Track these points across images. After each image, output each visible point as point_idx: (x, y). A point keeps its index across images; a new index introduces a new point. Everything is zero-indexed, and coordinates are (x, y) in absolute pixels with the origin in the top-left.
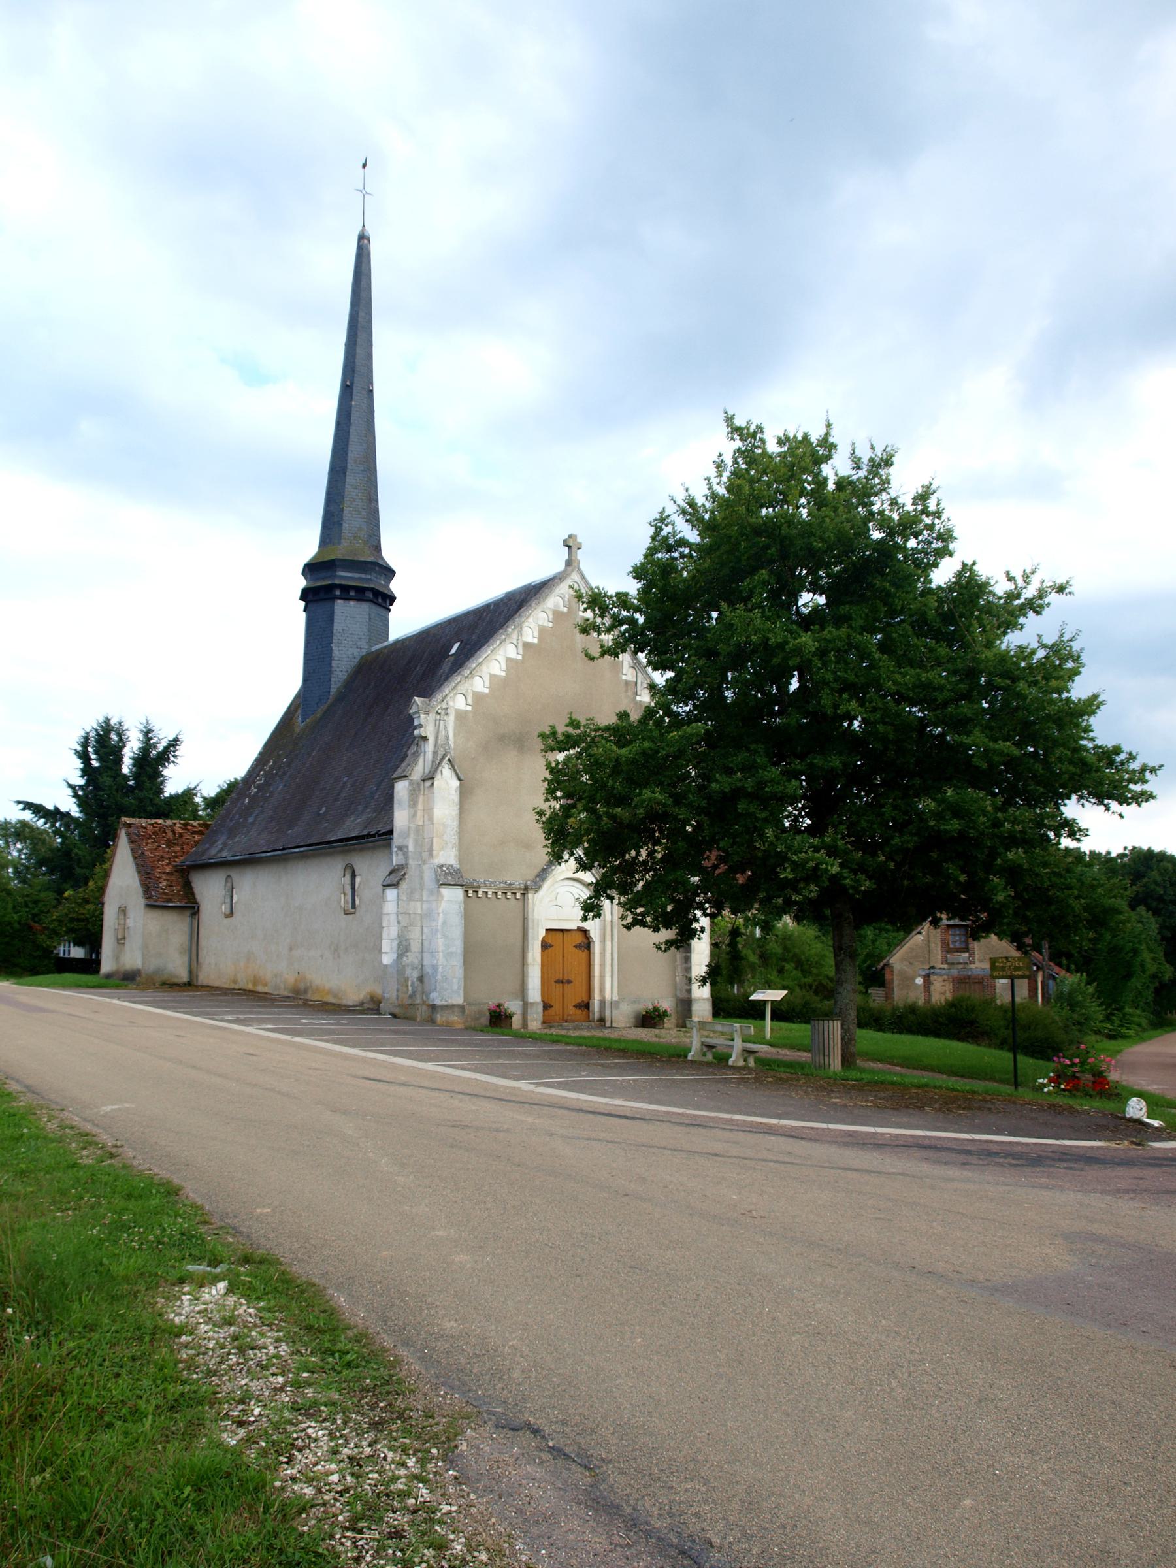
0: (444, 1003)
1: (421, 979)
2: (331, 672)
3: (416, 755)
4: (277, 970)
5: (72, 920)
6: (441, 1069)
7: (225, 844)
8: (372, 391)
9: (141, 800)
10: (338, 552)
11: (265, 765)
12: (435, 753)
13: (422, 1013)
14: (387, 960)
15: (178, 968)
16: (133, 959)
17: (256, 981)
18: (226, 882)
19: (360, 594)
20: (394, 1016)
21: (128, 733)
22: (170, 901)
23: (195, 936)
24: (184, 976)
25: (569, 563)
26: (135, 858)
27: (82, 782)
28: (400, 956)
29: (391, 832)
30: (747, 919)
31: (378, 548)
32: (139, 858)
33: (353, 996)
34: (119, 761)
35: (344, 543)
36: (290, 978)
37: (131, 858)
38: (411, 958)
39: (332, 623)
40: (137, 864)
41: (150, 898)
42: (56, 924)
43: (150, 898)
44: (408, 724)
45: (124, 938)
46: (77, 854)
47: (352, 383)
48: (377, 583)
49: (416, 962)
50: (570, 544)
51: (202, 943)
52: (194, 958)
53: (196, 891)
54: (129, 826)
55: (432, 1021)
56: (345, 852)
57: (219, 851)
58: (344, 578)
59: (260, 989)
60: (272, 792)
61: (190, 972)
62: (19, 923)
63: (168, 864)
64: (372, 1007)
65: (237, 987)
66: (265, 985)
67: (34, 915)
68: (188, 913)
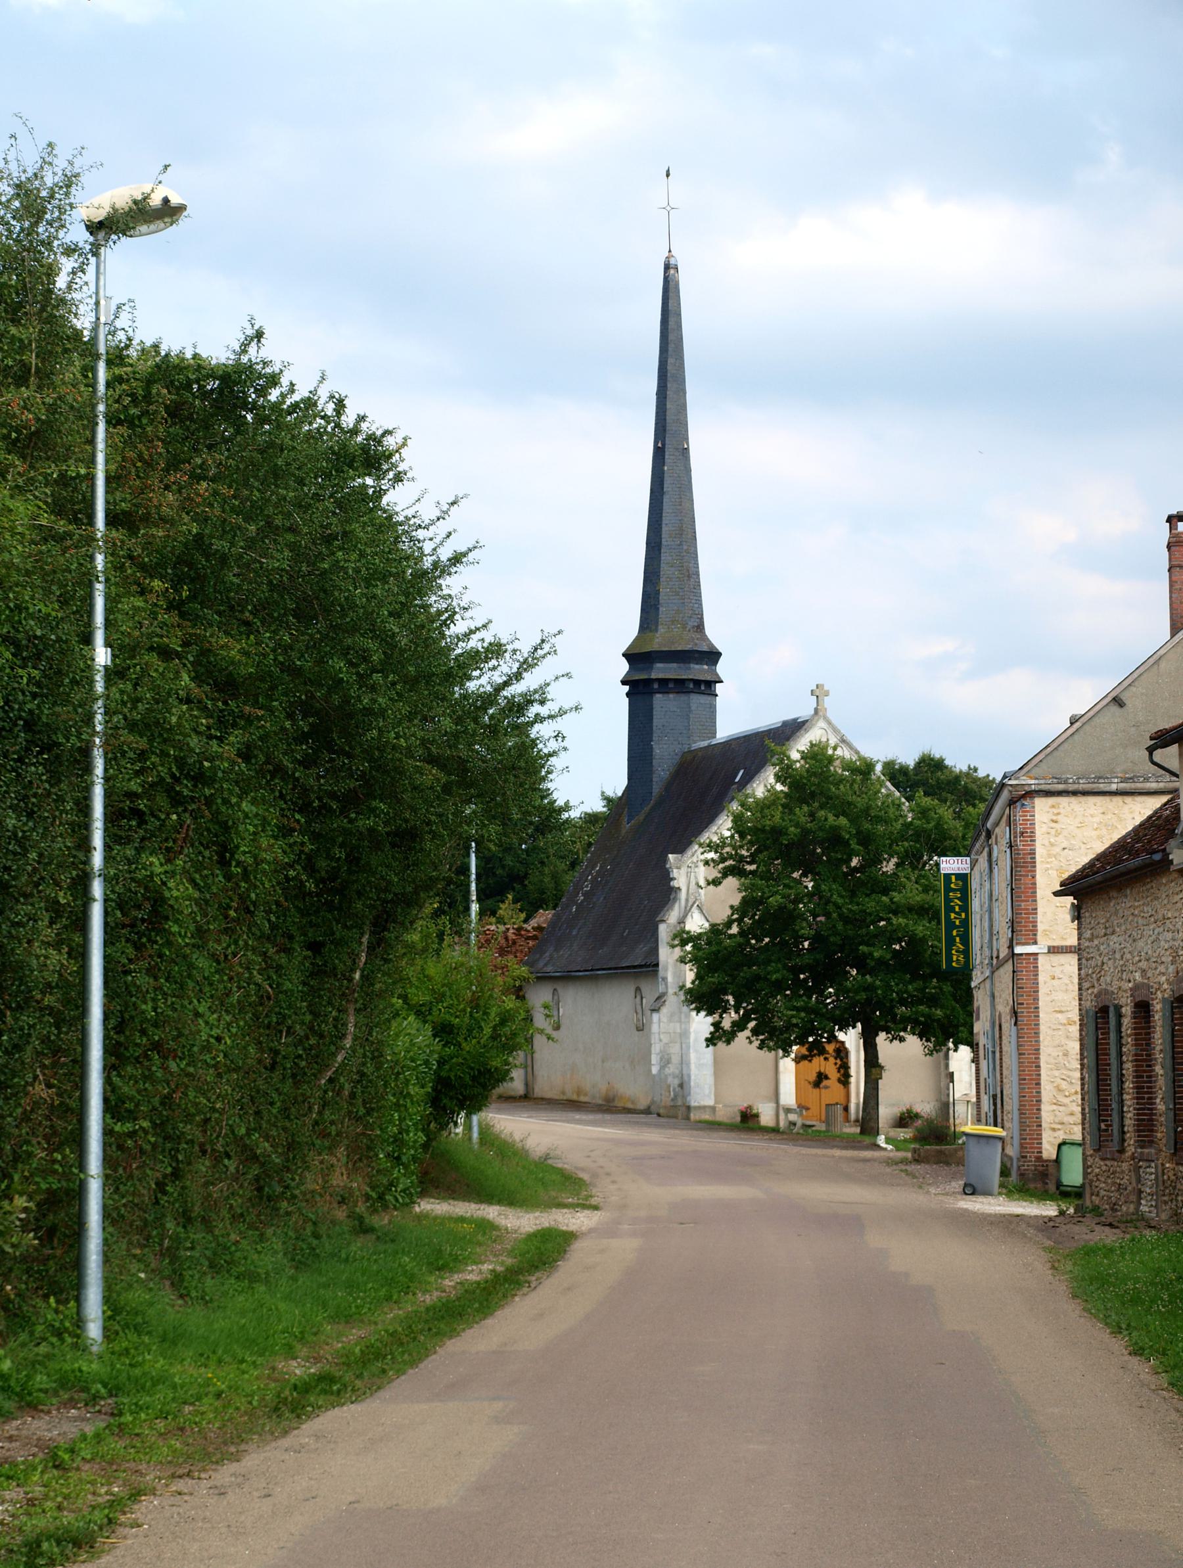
1: (681, 1086)
2: (651, 772)
3: (675, 899)
4: (594, 1083)
7: (551, 957)
8: (687, 449)
10: (658, 642)
11: (593, 868)
12: (687, 900)
13: (681, 1112)
14: (655, 1070)
19: (680, 686)
20: (659, 1115)
25: (816, 711)
28: (662, 1068)
29: (657, 965)
30: (829, 1042)
31: (700, 627)
33: (642, 1104)
35: (662, 629)
36: (603, 1087)
38: (672, 1069)
39: (652, 719)
44: (666, 877)
47: (664, 445)
48: (698, 671)
49: (677, 1072)
50: (818, 693)
52: (999, 1106)
55: (688, 1118)
56: (637, 976)
57: (546, 965)
59: (583, 1099)
61: (527, 1085)
64: (647, 1111)
66: (586, 1095)
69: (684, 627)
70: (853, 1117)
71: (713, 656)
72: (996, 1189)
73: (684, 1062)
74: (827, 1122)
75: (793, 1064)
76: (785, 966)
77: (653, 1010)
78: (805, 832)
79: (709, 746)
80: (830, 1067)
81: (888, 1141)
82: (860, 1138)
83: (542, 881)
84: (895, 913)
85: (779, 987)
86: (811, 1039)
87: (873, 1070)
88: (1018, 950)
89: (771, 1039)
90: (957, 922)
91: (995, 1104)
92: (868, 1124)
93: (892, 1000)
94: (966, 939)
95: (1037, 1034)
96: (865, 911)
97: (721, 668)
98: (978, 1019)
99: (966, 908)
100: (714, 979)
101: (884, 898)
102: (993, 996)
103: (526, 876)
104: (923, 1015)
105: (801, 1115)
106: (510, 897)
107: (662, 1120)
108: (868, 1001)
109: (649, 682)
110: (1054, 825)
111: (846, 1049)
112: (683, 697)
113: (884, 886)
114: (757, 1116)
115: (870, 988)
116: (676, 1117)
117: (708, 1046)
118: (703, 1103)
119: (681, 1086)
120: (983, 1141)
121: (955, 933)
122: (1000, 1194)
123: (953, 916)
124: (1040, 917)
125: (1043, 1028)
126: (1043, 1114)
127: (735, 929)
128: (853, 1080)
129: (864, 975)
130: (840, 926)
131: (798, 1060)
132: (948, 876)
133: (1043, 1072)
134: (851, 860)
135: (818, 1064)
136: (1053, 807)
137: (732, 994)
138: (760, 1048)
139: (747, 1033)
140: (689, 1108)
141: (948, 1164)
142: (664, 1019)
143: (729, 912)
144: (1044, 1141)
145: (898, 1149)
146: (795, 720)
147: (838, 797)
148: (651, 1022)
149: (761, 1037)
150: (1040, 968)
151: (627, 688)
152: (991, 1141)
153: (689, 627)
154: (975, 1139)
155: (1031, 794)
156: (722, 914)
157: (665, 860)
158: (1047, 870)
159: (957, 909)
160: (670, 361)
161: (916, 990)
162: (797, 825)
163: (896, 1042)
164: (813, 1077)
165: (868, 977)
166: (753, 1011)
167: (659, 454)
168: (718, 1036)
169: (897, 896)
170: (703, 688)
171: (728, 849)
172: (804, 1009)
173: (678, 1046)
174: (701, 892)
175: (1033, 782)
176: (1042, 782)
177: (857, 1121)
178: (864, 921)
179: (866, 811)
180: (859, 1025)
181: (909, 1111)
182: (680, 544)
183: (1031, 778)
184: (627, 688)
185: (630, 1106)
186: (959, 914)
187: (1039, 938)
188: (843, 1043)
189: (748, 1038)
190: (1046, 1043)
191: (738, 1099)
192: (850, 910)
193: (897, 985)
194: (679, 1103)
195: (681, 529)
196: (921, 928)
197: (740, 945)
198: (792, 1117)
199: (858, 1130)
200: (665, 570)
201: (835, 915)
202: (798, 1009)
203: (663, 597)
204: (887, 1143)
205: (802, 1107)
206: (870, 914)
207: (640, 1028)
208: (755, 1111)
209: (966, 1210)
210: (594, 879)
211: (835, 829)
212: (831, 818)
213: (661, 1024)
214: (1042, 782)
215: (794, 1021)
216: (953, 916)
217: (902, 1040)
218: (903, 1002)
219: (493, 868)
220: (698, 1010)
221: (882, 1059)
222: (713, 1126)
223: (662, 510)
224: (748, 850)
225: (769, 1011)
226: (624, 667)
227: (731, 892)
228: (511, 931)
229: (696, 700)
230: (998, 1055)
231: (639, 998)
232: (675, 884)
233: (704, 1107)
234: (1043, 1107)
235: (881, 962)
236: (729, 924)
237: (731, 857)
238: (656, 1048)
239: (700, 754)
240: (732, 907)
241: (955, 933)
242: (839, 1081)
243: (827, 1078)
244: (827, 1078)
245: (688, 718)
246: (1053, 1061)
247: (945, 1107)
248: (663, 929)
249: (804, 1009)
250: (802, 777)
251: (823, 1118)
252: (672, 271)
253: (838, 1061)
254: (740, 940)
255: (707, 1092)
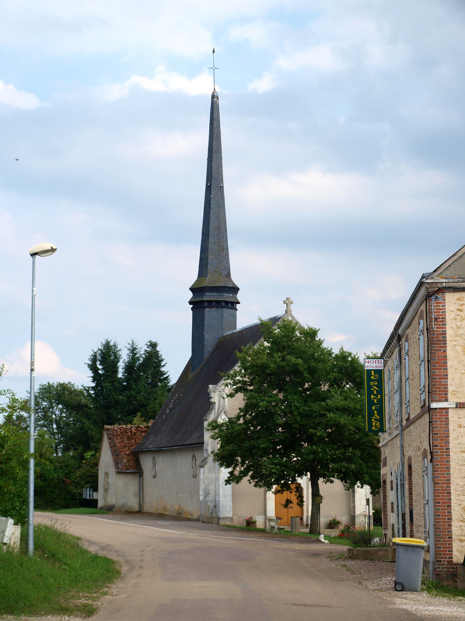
0: (223, 516)
1: (215, 506)
2: (203, 347)
3: (213, 409)
4: (172, 504)
5: (88, 477)
6: (173, 532)
8: (222, 187)
9: (129, 397)
10: (207, 283)
11: (174, 396)
12: (219, 409)
13: (215, 520)
14: (201, 498)
15: (134, 504)
16: (111, 500)
17: (165, 509)
18: (153, 460)
19: (218, 304)
20: (203, 522)
21: (120, 353)
22: (128, 469)
23: (141, 487)
24: (136, 508)
25: (286, 311)
26: (111, 447)
27: (93, 385)
29: (203, 443)
31: (228, 275)
32: (113, 446)
33: (195, 517)
34: (116, 372)
35: (209, 276)
36: (176, 507)
37: (109, 448)
38: (210, 498)
39: (204, 321)
40: (112, 451)
41: (118, 468)
42: (79, 479)
43: (118, 468)
45: (108, 489)
46: (90, 434)
47: (211, 184)
48: (227, 297)
49: (213, 499)
50: (288, 302)
51: (145, 491)
52: (141, 498)
53: (142, 464)
54: (108, 430)
55: (218, 524)
57: (149, 444)
58: (212, 295)
59: (167, 513)
60: (174, 413)
61: (140, 506)
62: (58, 479)
63: (128, 450)
64: (198, 520)
65: (158, 513)
66: (168, 511)
67: (66, 474)
68: (138, 475)
69: (220, 275)
70: (305, 523)
71: (235, 290)
72: (420, 586)
73: (216, 494)
74: (291, 526)
75: (273, 496)
76: (269, 441)
77: (201, 467)
78: (279, 367)
79: (232, 333)
80: (293, 497)
81: (326, 537)
82: (309, 536)
83: (154, 407)
84: (329, 411)
85: (265, 452)
86: (282, 482)
87: (317, 498)
88: (434, 405)
89: (261, 481)
90: (375, 401)
91: (404, 519)
92: (314, 529)
93: (327, 459)
94: (381, 412)
95: (448, 468)
96: (312, 410)
97: (239, 296)
98: (385, 465)
99: (381, 391)
100: (230, 447)
101: (322, 403)
102: (402, 446)
103: (147, 404)
104: (344, 468)
105: (277, 523)
106: (139, 414)
107: (204, 525)
108: (314, 460)
109: (202, 302)
110: (459, 313)
111: (301, 487)
112: (220, 310)
113: (322, 397)
114: (255, 522)
115: (315, 453)
116: (212, 523)
117: (226, 484)
118: (226, 516)
119: (215, 506)
120: (410, 549)
121: (374, 408)
122: (422, 590)
123: (372, 397)
124: (450, 381)
125: (453, 464)
126: (453, 528)
127: (241, 421)
128: (305, 504)
129: (312, 446)
130: (298, 418)
131: (276, 493)
132: (369, 371)
133: (453, 497)
134: (304, 385)
135: (286, 495)
136: (459, 299)
137: (240, 456)
138: (255, 486)
139: (248, 478)
140: (219, 518)
141: (372, 559)
142: (206, 471)
143: (239, 411)
144: (454, 549)
145: (331, 543)
146: (275, 317)
147: (297, 348)
148: (199, 473)
149: (256, 480)
150: (450, 419)
151: (192, 306)
152: (416, 549)
153: (223, 275)
154: (404, 548)
155: (442, 290)
156: (234, 413)
157: (208, 387)
158: (455, 346)
159: (375, 392)
160: (214, 143)
161: (340, 453)
162: (275, 363)
163: (329, 483)
164: (284, 502)
165: (314, 446)
166: (251, 466)
167: (208, 189)
168: (233, 479)
169: (329, 402)
170: (230, 305)
171: (238, 378)
172: (280, 464)
173: (214, 485)
174: (225, 402)
175: (444, 281)
176: (451, 280)
177: (307, 525)
178: (312, 415)
179: (313, 356)
180: (309, 473)
181: (334, 520)
182: (219, 234)
183: (443, 278)
184: (192, 306)
185: (189, 517)
186: (376, 395)
187: (449, 396)
188: (300, 484)
189: (249, 480)
190: (455, 475)
191: (245, 513)
192: (304, 410)
193: (330, 451)
194: (214, 516)
195: (219, 226)
196: (344, 419)
197: (244, 429)
198: (272, 524)
199: (308, 530)
200: (211, 246)
201: (296, 413)
202: (275, 464)
203: (210, 260)
204: (325, 539)
205: (278, 518)
206: (315, 412)
207: (195, 477)
208: (254, 520)
209: (407, 612)
210: (175, 401)
211: (296, 365)
212: (293, 359)
213: (205, 474)
214: (451, 280)
215: (273, 471)
216: (372, 397)
217: (332, 482)
218: (333, 461)
219: (132, 401)
220: (221, 465)
221: (321, 493)
222: (231, 528)
223: (209, 217)
224: (249, 378)
225: (260, 465)
226: (190, 295)
227: (240, 400)
228: (134, 428)
229: (227, 312)
230: (407, 486)
231: (194, 461)
232: (212, 400)
233: (227, 518)
234: (453, 523)
235: (321, 438)
236: (238, 418)
237: (239, 381)
238: (202, 487)
239: (228, 338)
240: (240, 409)
241: (374, 408)
242: (298, 504)
243: (291, 502)
244: (291, 502)
245: (222, 320)
246: (460, 489)
247: (353, 518)
248: (206, 424)
249: (280, 464)
250: (278, 337)
251: (289, 524)
252: (215, 99)
253: (297, 493)
254: (244, 426)
255: (228, 510)
